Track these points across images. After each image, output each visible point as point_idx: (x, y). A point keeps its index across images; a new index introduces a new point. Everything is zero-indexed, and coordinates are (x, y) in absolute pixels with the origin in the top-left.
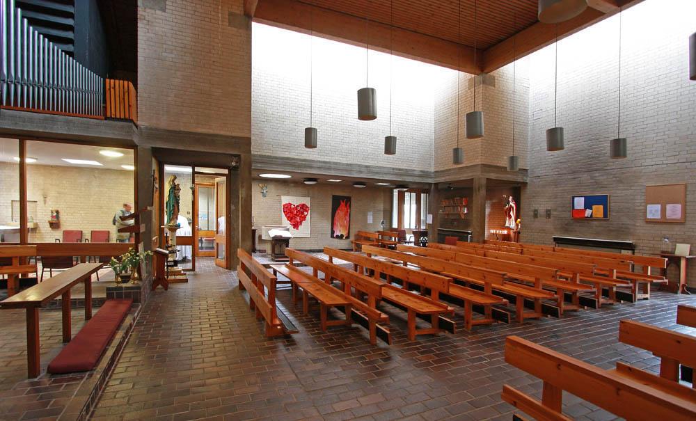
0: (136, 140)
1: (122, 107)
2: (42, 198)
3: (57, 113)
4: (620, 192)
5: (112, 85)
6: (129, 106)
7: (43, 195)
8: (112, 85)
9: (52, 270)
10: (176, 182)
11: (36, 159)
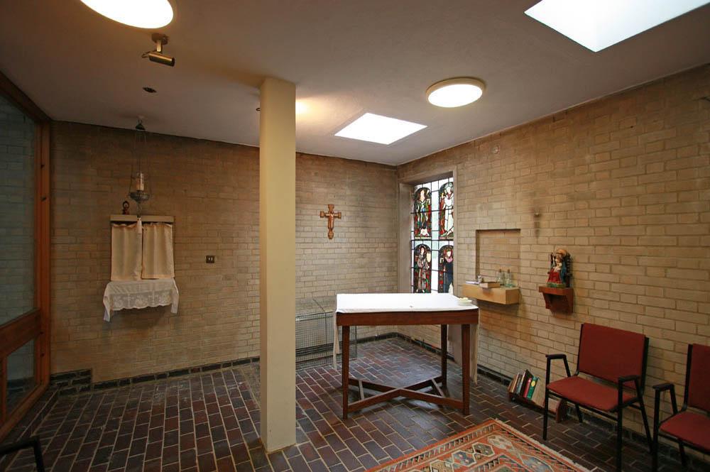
2: (530, 220)
7: (533, 210)
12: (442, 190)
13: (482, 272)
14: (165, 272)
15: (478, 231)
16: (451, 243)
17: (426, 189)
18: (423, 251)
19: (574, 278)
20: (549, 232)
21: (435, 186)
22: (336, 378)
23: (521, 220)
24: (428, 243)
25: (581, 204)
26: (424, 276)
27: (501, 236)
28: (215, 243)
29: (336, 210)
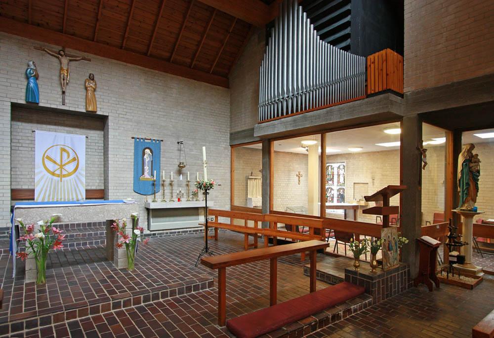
0: (395, 111)
1: (380, 77)
2: (371, 180)
3: (274, 119)
4: (367, 220)
5: (5, 180)
6: (387, 75)
7: (372, 178)
8: (5, 180)
9: (338, 241)
10: (474, 152)
11: (362, 147)
12: (339, 167)
13: (355, 197)
14: (259, 195)
15: (354, 183)
16: (343, 187)
17: (332, 166)
18: (330, 190)
19: (43, 55)
20: (376, 184)
21: (335, 166)
22: (215, 314)
23: (369, 180)
24: (332, 187)
25: (385, 177)
26: (330, 200)
27: (362, 185)
28: (17, 182)
29: (301, 174)
